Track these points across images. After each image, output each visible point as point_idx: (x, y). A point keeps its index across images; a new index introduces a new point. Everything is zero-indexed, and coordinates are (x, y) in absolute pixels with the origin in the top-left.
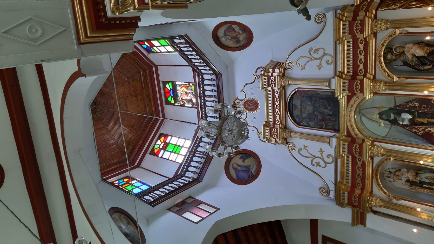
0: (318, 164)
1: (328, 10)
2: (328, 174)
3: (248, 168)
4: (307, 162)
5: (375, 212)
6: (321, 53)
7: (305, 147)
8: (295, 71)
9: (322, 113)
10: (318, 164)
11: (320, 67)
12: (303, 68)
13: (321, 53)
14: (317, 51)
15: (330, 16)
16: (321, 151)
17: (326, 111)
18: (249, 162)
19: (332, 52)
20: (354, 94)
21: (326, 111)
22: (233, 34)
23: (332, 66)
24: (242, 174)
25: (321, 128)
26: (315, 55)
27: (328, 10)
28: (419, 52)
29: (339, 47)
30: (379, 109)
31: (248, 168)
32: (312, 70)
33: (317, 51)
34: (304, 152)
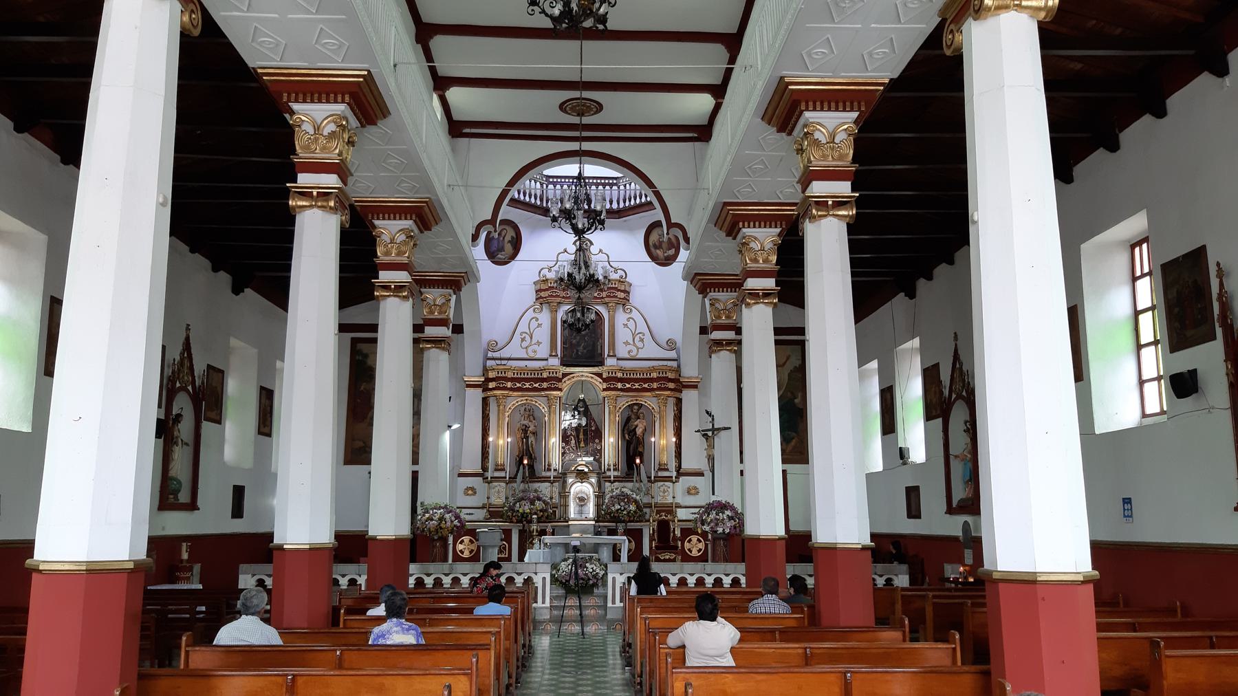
0: (523, 340)
1: (678, 353)
2: (514, 350)
3: (502, 249)
4: (523, 327)
5: (485, 401)
6: (640, 344)
7: (540, 325)
8: (621, 317)
9: (578, 344)
10: (523, 340)
11: (627, 343)
12: (625, 325)
13: (640, 344)
14: (642, 340)
15: (673, 354)
16: (539, 343)
17: (581, 348)
18: (509, 248)
19: (639, 356)
20: (605, 380)
21: (581, 348)
22: (664, 246)
23: (627, 356)
24: (495, 244)
25: (564, 343)
26: (637, 339)
27: (678, 353)
28: (639, 431)
29: (618, 108)
30: (658, 512)
31: (502, 249)
32: (623, 335)
33: (642, 340)
34: (534, 324)
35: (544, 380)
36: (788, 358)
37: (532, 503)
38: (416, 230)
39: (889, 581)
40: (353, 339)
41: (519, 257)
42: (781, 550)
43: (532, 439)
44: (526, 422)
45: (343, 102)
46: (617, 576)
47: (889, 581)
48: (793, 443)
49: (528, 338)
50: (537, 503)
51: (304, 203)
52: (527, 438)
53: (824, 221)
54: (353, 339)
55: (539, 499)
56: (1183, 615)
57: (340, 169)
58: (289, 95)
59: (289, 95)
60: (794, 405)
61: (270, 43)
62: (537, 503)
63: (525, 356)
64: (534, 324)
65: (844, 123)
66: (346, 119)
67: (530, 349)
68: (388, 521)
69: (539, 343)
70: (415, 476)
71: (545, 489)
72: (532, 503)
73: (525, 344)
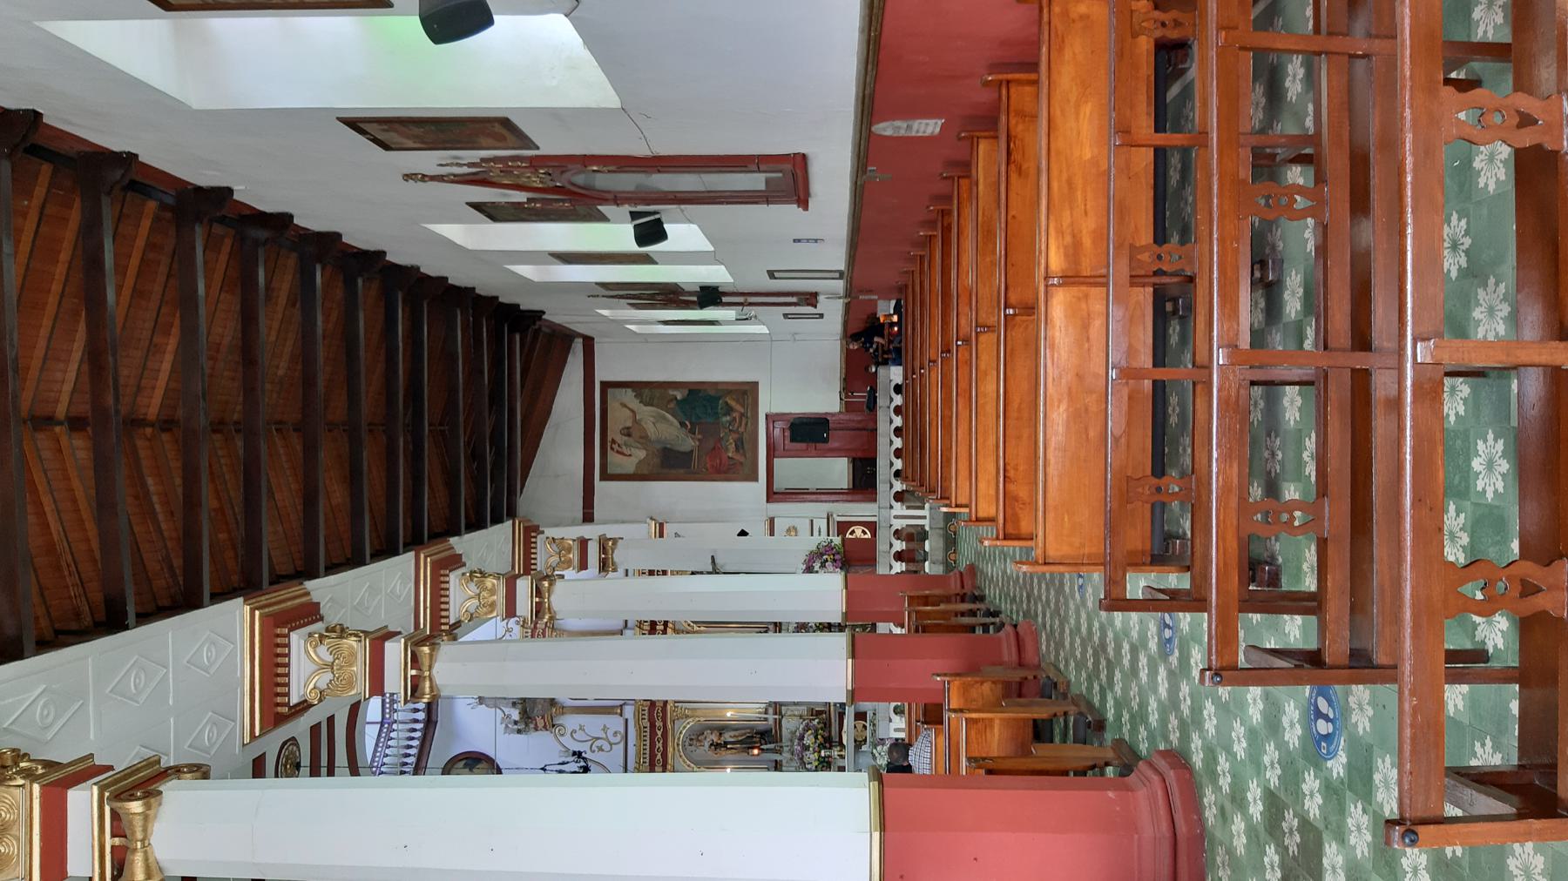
0: (600, 749)
7: (582, 728)
10: (600, 749)
34: (579, 735)
35: (653, 726)
36: (624, 405)
37: (806, 748)
38: (463, 570)
39: (898, 389)
40: (602, 479)
41: (491, 754)
42: (860, 573)
43: (727, 737)
44: (707, 744)
45: (288, 636)
46: (893, 726)
47: (898, 389)
48: (733, 403)
49: (599, 743)
50: (807, 741)
51: (427, 684)
52: (726, 743)
53: (438, 680)
54: (602, 479)
55: (802, 738)
56: (935, 229)
57: (379, 639)
58: (278, 705)
59: (278, 705)
60: (684, 400)
61: (209, 650)
62: (807, 741)
63: (622, 745)
64: (579, 735)
65: (307, 652)
66: (310, 635)
67: (613, 740)
68: (827, 592)
69: (605, 729)
70: (778, 627)
71: (790, 725)
72: (806, 748)
73: (606, 747)
